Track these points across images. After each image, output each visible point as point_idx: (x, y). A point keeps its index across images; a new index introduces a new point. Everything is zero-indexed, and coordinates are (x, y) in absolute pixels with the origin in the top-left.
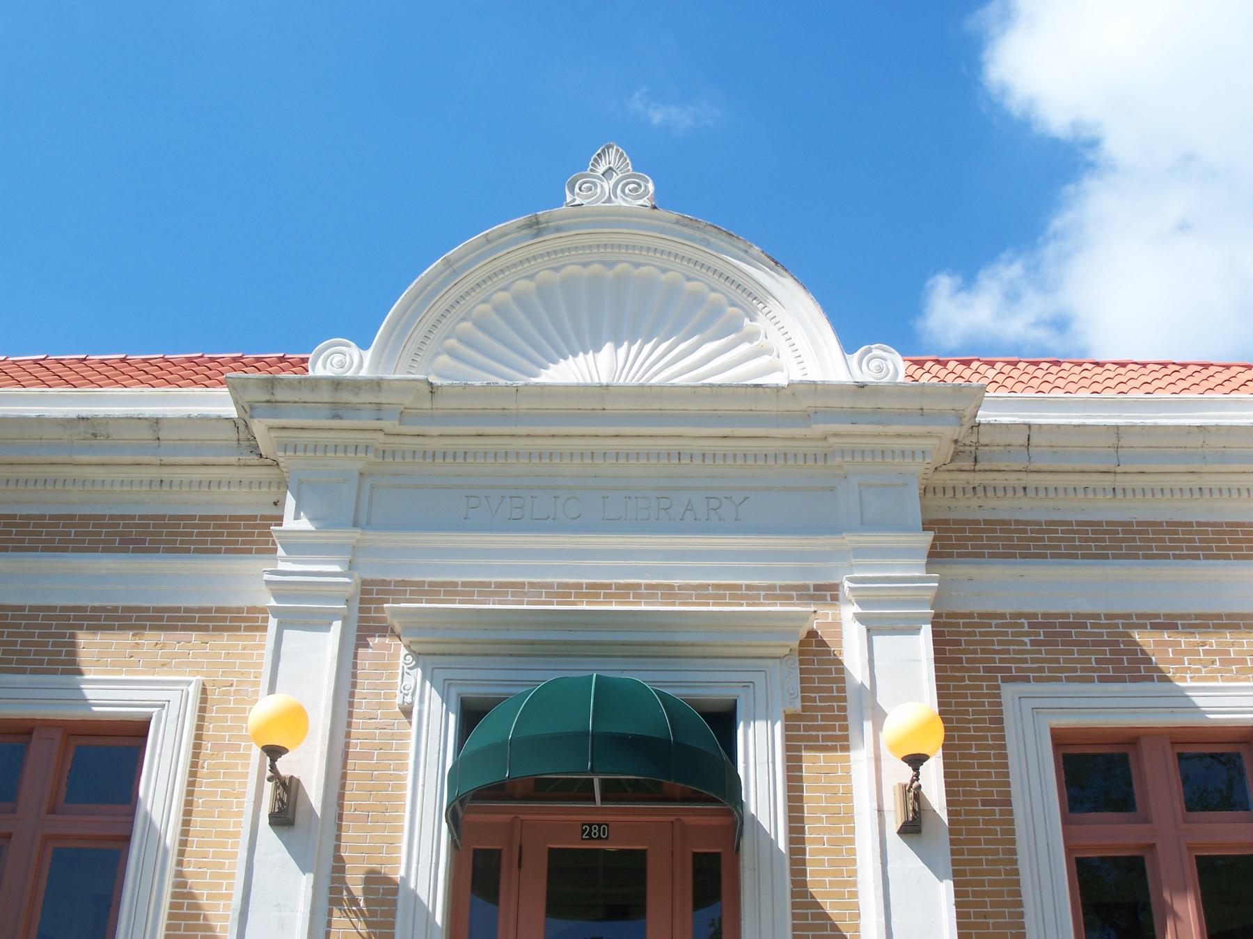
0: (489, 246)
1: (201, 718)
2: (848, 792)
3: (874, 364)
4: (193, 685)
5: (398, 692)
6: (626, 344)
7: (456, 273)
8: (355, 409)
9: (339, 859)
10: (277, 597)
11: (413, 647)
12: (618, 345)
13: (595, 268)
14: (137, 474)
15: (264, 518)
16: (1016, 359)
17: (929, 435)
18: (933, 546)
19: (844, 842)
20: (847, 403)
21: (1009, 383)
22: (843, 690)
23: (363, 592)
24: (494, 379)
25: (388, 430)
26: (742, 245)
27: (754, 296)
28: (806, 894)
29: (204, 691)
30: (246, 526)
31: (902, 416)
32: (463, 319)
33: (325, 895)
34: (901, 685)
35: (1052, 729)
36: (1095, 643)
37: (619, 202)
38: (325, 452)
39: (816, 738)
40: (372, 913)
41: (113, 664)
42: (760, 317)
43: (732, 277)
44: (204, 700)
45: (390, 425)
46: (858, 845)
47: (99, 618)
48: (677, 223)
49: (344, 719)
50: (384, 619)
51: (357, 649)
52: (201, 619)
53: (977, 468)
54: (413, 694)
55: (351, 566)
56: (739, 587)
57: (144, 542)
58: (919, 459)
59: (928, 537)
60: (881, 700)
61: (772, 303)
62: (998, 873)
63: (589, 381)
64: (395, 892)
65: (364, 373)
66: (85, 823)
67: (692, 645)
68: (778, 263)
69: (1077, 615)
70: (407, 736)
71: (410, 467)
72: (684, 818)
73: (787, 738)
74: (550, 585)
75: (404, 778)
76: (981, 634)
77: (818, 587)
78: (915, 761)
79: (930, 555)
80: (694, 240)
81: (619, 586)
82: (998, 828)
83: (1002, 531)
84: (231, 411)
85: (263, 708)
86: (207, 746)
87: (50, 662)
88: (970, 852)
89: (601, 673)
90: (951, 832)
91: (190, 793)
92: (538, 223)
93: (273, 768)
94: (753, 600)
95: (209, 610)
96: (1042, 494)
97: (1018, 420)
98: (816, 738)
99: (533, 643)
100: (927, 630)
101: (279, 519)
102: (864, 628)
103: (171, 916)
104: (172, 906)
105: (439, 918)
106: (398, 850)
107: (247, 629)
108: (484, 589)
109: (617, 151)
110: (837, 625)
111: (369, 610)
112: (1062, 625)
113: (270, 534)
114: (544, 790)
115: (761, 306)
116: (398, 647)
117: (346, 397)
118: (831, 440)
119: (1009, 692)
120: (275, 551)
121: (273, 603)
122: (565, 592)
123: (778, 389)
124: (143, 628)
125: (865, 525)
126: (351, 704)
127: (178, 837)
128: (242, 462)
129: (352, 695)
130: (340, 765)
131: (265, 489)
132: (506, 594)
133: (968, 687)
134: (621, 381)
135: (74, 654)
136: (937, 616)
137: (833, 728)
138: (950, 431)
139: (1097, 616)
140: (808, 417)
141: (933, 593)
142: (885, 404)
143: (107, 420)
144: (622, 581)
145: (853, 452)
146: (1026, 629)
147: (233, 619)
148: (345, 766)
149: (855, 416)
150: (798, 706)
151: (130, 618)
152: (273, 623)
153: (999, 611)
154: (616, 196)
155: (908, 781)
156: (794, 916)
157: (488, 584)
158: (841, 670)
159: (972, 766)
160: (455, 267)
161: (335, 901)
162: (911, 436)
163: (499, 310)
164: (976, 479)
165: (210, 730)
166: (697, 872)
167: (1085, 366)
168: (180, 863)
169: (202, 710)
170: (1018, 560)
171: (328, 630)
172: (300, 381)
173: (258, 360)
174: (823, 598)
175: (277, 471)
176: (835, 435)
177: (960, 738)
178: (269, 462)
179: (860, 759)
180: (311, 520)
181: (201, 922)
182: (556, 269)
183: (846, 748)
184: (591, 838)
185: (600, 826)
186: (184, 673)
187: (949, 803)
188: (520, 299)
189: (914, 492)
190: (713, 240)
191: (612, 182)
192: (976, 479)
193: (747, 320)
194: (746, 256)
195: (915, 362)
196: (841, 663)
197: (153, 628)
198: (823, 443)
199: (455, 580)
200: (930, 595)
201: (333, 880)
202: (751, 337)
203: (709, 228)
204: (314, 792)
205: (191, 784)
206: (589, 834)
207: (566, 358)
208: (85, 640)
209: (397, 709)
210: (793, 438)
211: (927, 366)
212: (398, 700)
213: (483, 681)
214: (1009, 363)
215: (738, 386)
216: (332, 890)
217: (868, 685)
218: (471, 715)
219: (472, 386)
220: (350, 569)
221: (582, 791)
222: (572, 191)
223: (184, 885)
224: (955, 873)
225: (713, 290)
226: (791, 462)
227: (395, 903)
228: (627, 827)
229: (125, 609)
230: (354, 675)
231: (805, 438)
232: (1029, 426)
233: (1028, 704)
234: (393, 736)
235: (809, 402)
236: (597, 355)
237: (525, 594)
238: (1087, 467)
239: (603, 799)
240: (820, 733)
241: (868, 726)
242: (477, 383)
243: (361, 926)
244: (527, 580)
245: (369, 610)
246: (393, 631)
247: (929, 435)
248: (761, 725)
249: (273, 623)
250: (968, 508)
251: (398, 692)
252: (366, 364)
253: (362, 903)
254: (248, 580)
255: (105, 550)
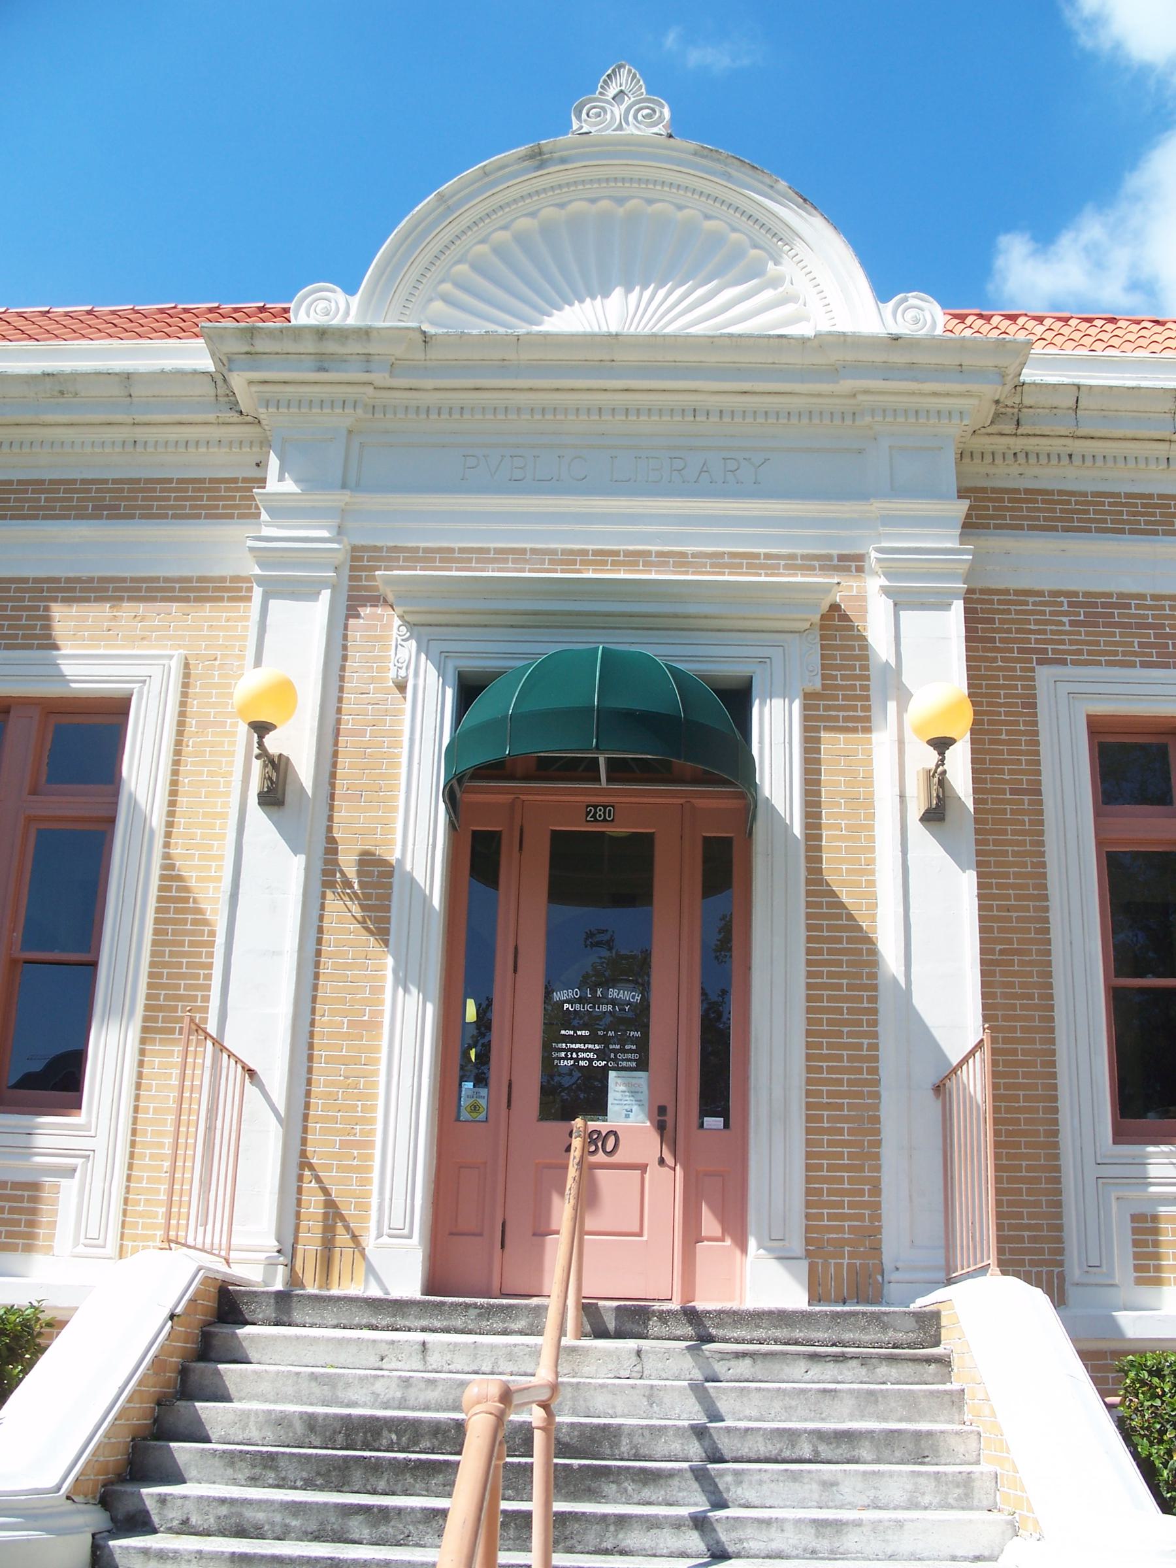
0: (486, 180)
1: (185, 694)
2: (869, 776)
3: (910, 314)
4: (175, 659)
5: (391, 665)
6: (638, 289)
7: (450, 210)
8: (341, 361)
9: (331, 840)
10: (262, 565)
11: (407, 618)
12: (629, 290)
13: (605, 204)
14: (110, 434)
15: (245, 480)
16: (1067, 314)
17: (968, 394)
18: (968, 516)
19: (863, 829)
20: (879, 357)
21: (1059, 340)
22: (866, 668)
23: (353, 559)
24: (492, 327)
25: (378, 383)
26: (767, 180)
27: (778, 237)
28: (821, 882)
29: (187, 665)
30: (227, 489)
31: (939, 373)
32: (459, 262)
33: (318, 877)
34: (928, 662)
35: (1088, 716)
36: (1140, 626)
37: (631, 130)
38: (311, 408)
39: (836, 719)
40: (367, 896)
41: (91, 638)
42: (786, 260)
43: (757, 215)
44: (187, 675)
45: (380, 377)
46: (877, 832)
47: (73, 590)
48: (695, 154)
49: (334, 693)
50: (376, 588)
51: (347, 619)
52: (182, 590)
53: (1020, 431)
54: (407, 668)
55: (340, 531)
56: (756, 556)
57: (118, 507)
58: (956, 421)
59: (963, 506)
60: (906, 679)
61: (799, 246)
62: (1033, 1041)
63: (596, 329)
64: (391, 874)
65: (351, 321)
66: (69, 804)
67: (706, 617)
68: (807, 200)
69: (1121, 595)
70: (401, 712)
71: (402, 422)
72: (696, 801)
73: (806, 718)
74: (553, 552)
75: (399, 756)
76: (1017, 612)
77: (841, 558)
78: (942, 745)
79: (965, 526)
80: (714, 173)
81: (628, 553)
82: (1026, 819)
83: (1044, 501)
84: (207, 364)
85: (249, 683)
86: (192, 724)
87: (24, 637)
88: (996, 843)
89: (607, 646)
90: (977, 821)
91: (175, 773)
92: (541, 154)
93: (261, 745)
94: (772, 569)
95: (188, 580)
96: (1089, 462)
97: (1066, 381)
98: (836, 719)
99: (536, 613)
100: (958, 606)
101: (262, 482)
102: (891, 603)
103: (160, 899)
104: (161, 888)
105: (436, 901)
106: (392, 831)
107: (231, 599)
108: (483, 556)
109: (630, 71)
110: (862, 598)
111: (359, 578)
112: (1104, 605)
113: (252, 498)
114: (549, 769)
115: (787, 248)
116: (390, 617)
117: (331, 347)
118: (861, 398)
119: (1044, 675)
120: (258, 515)
121: (257, 571)
122: (570, 558)
123: (804, 340)
124: (121, 599)
125: (896, 491)
126: (342, 678)
127: (164, 818)
128: (221, 420)
129: (343, 668)
130: (331, 741)
131: (246, 449)
132: (506, 561)
133: (1000, 669)
134: (632, 330)
135: (48, 627)
136: (970, 591)
137: (854, 708)
138: (990, 390)
139: (1142, 597)
140: (835, 372)
141: (966, 566)
142: (921, 359)
143: (75, 376)
144: (631, 548)
145: (884, 411)
146: (1065, 608)
147: (216, 589)
148: (336, 743)
149: (887, 371)
150: (818, 686)
151: (107, 590)
152: (257, 592)
153: (1037, 588)
154: (627, 123)
155: (933, 767)
156: (809, 905)
157: (487, 551)
158: (865, 647)
159: (1001, 752)
160: (450, 202)
161: (329, 884)
162: (948, 395)
163: (499, 251)
164: (1018, 444)
165: (194, 706)
166: (706, 860)
167: (1144, 324)
168: (167, 845)
169: (185, 685)
170: (1060, 533)
171: (316, 600)
172: (281, 330)
173: (236, 310)
174: (847, 569)
175: (257, 429)
176: (866, 392)
177: (990, 722)
178: (249, 419)
179: (882, 741)
180: (296, 481)
181: (191, 905)
182: (562, 206)
183: (868, 730)
184: (596, 820)
185: (605, 807)
186: (164, 647)
187: (975, 791)
188: (521, 239)
189: (950, 457)
190: (734, 173)
191: (623, 107)
192: (1018, 444)
193: (771, 264)
194: (771, 191)
195: (955, 316)
196: (864, 639)
197: (131, 599)
198: (852, 401)
199: (452, 545)
200: (963, 569)
201: (326, 862)
202: (775, 282)
203: (730, 160)
204: (304, 770)
205: (176, 763)
206: (594, 816)
207: (571, 304)
208: (58, 611)
209: (391, 684)
210: (819, 395)
211: (969, 320)
212: (392, 674)
213: (481, 655)
214: (1059, 319)
215: (760, 337)
216: (325, 872)
217: (893, 663)
218: (469, 691)
219: (469, 334)
220: (339, 534)
221: (584, 770)
222: (579, 118)
223: (172, 867)
224: (979, 864)
225: (734, 230)
226: (816, 421)
227: (390, 886)
228: (632, 808)
229: (102, 580)
230: (345, 648)
231: (832, 395)
232: (1078, 387)
233: (1064, 688)
234: (386, 712)
235: (837, 355)
236: (608, 302)
237: (526, 561)
238: (1140, 434)
239: (609, 780)
240: (841, 714)
241: (892, 706)
242: (475, 332)
243: (355, 909)
244: (528, 546)
245: (359, 578)
246: (385, 601)
247: (968, 394)
248: (777, 703)
249: (257, 592)
250: (1007, 476)
251: (391, 665)
252: (353, 311)
253: (356, 886)
254: (230, 546)
255: (77, 517)
